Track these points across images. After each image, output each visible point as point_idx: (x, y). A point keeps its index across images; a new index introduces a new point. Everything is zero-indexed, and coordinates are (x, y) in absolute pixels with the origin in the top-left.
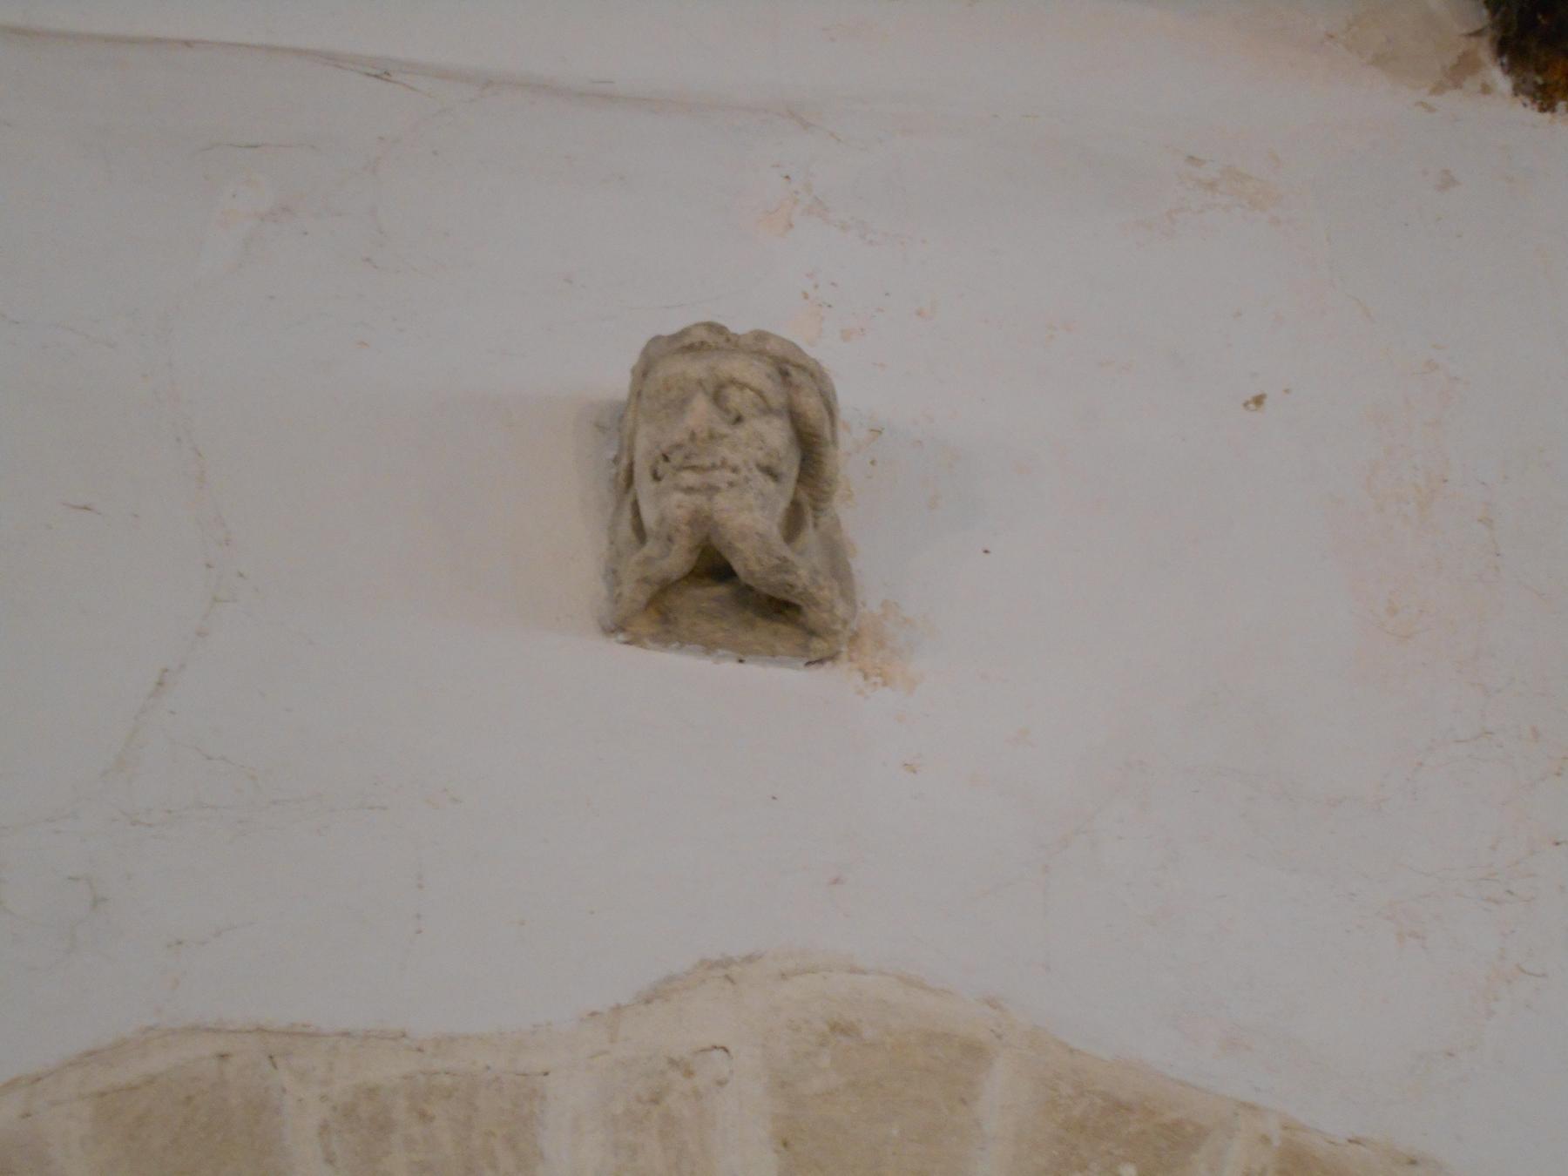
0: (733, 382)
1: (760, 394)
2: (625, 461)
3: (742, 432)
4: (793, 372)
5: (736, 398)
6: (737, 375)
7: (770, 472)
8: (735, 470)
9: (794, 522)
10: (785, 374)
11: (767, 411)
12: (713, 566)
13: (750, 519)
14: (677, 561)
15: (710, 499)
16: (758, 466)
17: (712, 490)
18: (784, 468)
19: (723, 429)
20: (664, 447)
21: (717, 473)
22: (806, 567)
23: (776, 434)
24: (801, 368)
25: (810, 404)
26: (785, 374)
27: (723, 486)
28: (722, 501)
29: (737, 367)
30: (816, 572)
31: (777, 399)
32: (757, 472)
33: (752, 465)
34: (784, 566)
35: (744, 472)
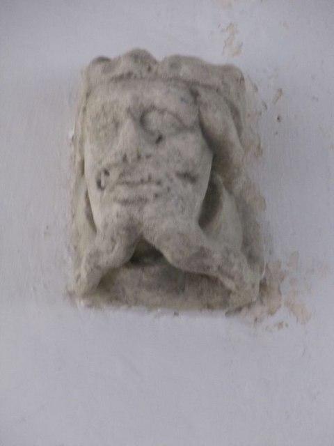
0: (153, 108)
1: (176, 116)
2: (78, 158)
3: (163, 151)
4: (202, 92)
5: (154, 119)
6: (157, 102)
7: (189, 177)
8: (159, 183)
9: (207, 215)
10: (195, 95)
11: (181, 128)
12: (142, 254)
13: (171, 224)
14: (114, 254)
15: (141, 209)
16: (179, 175)
17: (142, 201)
18: (199, 171)
19: (149, 150)
20: (104, 164)
21: (145, 187)
22: (221, 246)
23: (190, 147)
24: (245, 212)
25: (217, 119)
26: (195, 95)
27: (151, 197)
28: (149, 210)
29: (157, 95)
30: (228, 251)
31: (190, 119)
32: (178, 181)
33: (173, 176)
34: (202, 253)
35: (166, 184)
